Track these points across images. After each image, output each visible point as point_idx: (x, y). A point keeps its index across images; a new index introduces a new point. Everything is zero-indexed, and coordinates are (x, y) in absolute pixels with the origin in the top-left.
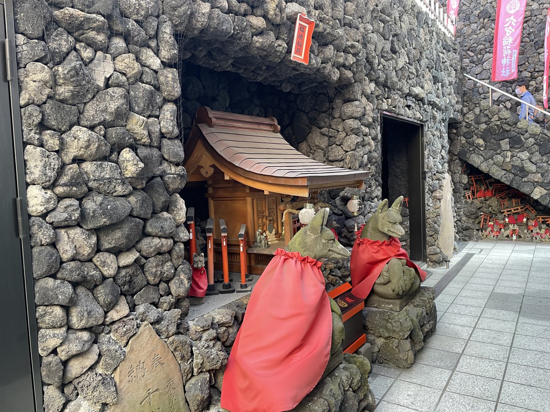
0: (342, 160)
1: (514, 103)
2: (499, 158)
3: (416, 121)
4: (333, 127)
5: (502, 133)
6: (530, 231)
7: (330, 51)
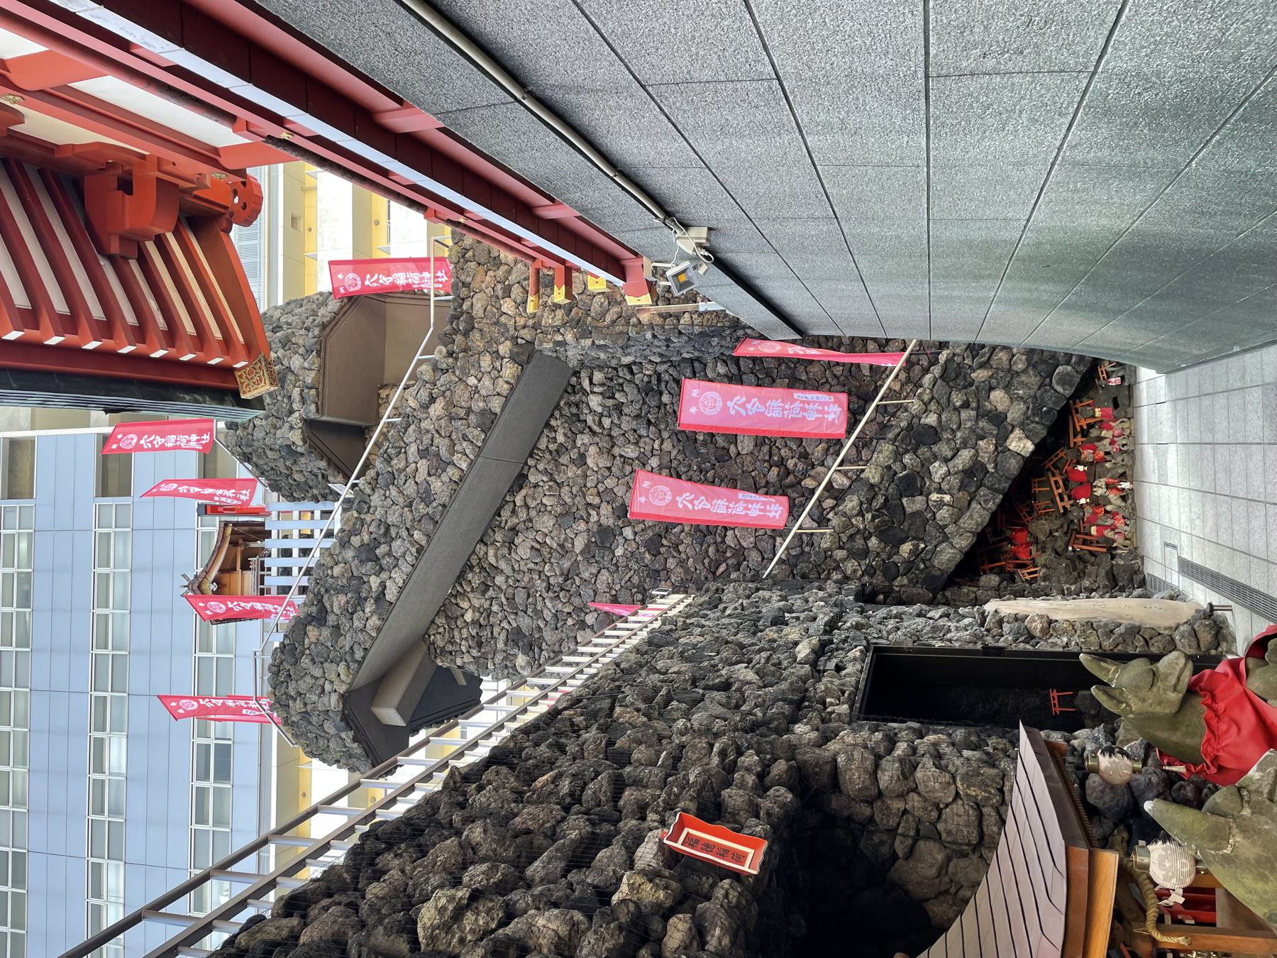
0: (978, 807)
1: (826, 494)
2: (943, 514)
3: (868, 660)
4: (892, 822)
5: (892, 508)
6: (1108, 458)
7: (734, 797)
